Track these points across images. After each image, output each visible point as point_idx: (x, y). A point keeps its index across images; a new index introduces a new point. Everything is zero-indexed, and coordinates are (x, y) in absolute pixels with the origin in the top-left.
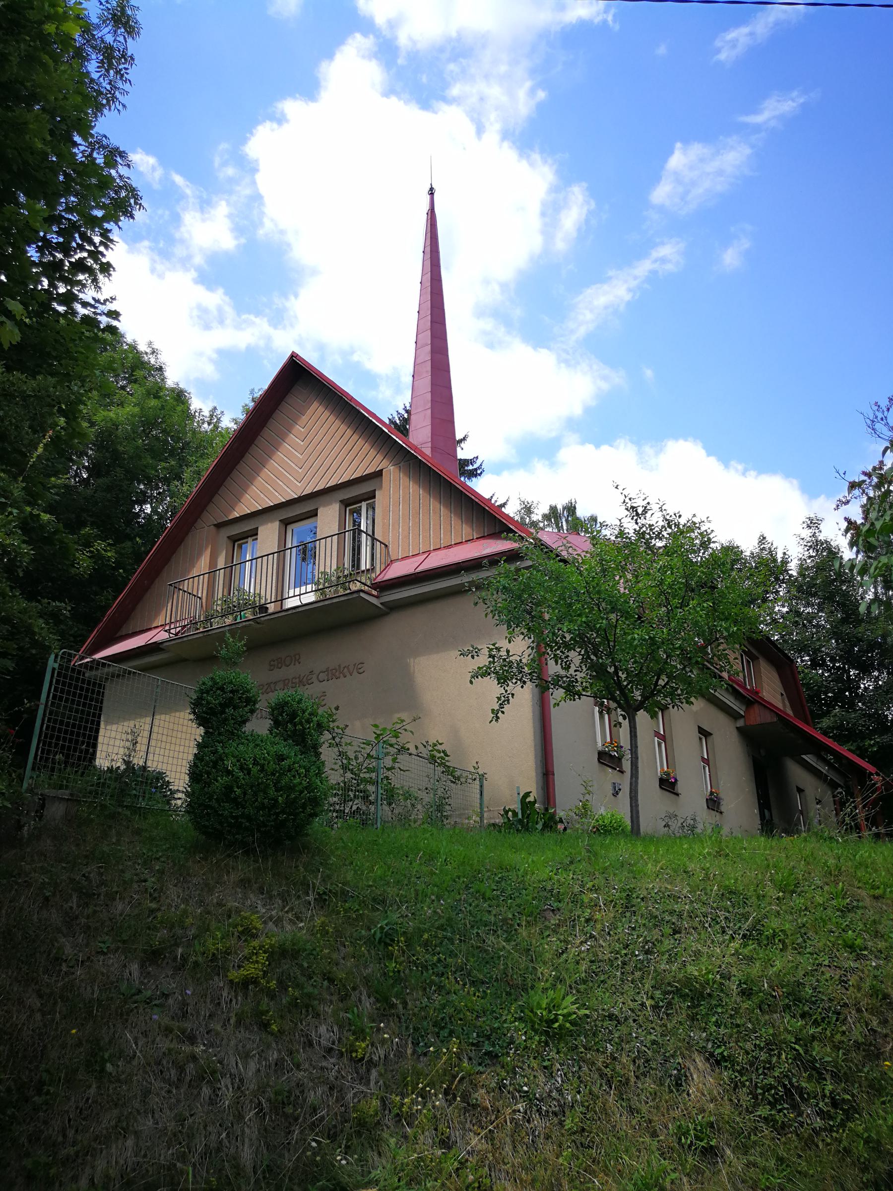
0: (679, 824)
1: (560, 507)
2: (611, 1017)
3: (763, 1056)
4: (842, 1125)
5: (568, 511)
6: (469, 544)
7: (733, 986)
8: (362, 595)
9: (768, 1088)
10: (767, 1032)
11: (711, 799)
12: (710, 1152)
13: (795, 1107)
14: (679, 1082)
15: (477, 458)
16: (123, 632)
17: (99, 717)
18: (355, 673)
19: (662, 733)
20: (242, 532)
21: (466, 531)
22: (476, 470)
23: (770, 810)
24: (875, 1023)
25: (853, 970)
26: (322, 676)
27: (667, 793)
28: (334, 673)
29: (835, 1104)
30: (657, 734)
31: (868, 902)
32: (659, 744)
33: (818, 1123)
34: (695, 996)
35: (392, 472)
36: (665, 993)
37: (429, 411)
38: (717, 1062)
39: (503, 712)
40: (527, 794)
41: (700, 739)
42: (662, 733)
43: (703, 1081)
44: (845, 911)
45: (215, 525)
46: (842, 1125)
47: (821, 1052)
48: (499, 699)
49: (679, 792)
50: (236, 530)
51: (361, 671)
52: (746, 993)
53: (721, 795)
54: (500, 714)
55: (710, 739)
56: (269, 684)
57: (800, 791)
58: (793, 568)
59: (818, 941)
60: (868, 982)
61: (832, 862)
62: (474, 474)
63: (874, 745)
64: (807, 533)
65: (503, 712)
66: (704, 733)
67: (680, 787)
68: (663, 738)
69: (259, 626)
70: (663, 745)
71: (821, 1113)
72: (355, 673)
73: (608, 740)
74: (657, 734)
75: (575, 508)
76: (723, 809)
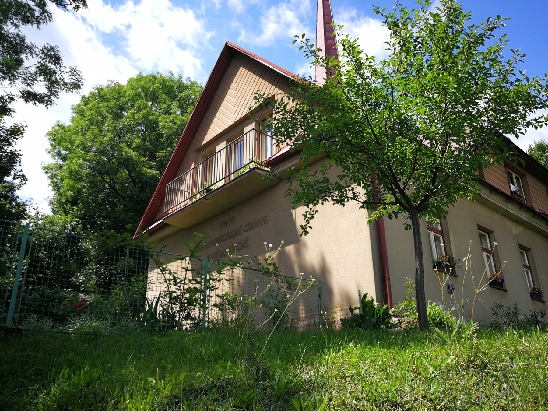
0: (505, 312)
8: (256, 170)
11: (534, 293)
16: (157, 219)
17: (148, 265)
18: (263, 223)
19: (528, 265)
20: (207, 154)
26: (246, 228)
27: (496, 290)
28: (252, 226)
30: (525, 266)
32: (527, 272)
39: (310, 227)
41: (522, 253)
42: (490, 249)
45: (196, 150)
48: (306, 216)
49: (507, 289)
50: (206, 151)
51: (266, 222)
53: (542, 290)
54: (308, 230)
55: (529, 253)
56: (220, 237)
65: (310, 227)
66: (524, 249)
68: (529, 268)
69: (208, 201)
70: (491, 258)
72: (263, 223)
73: (444, 254)
74: (525, 266)
76: (544, 299)
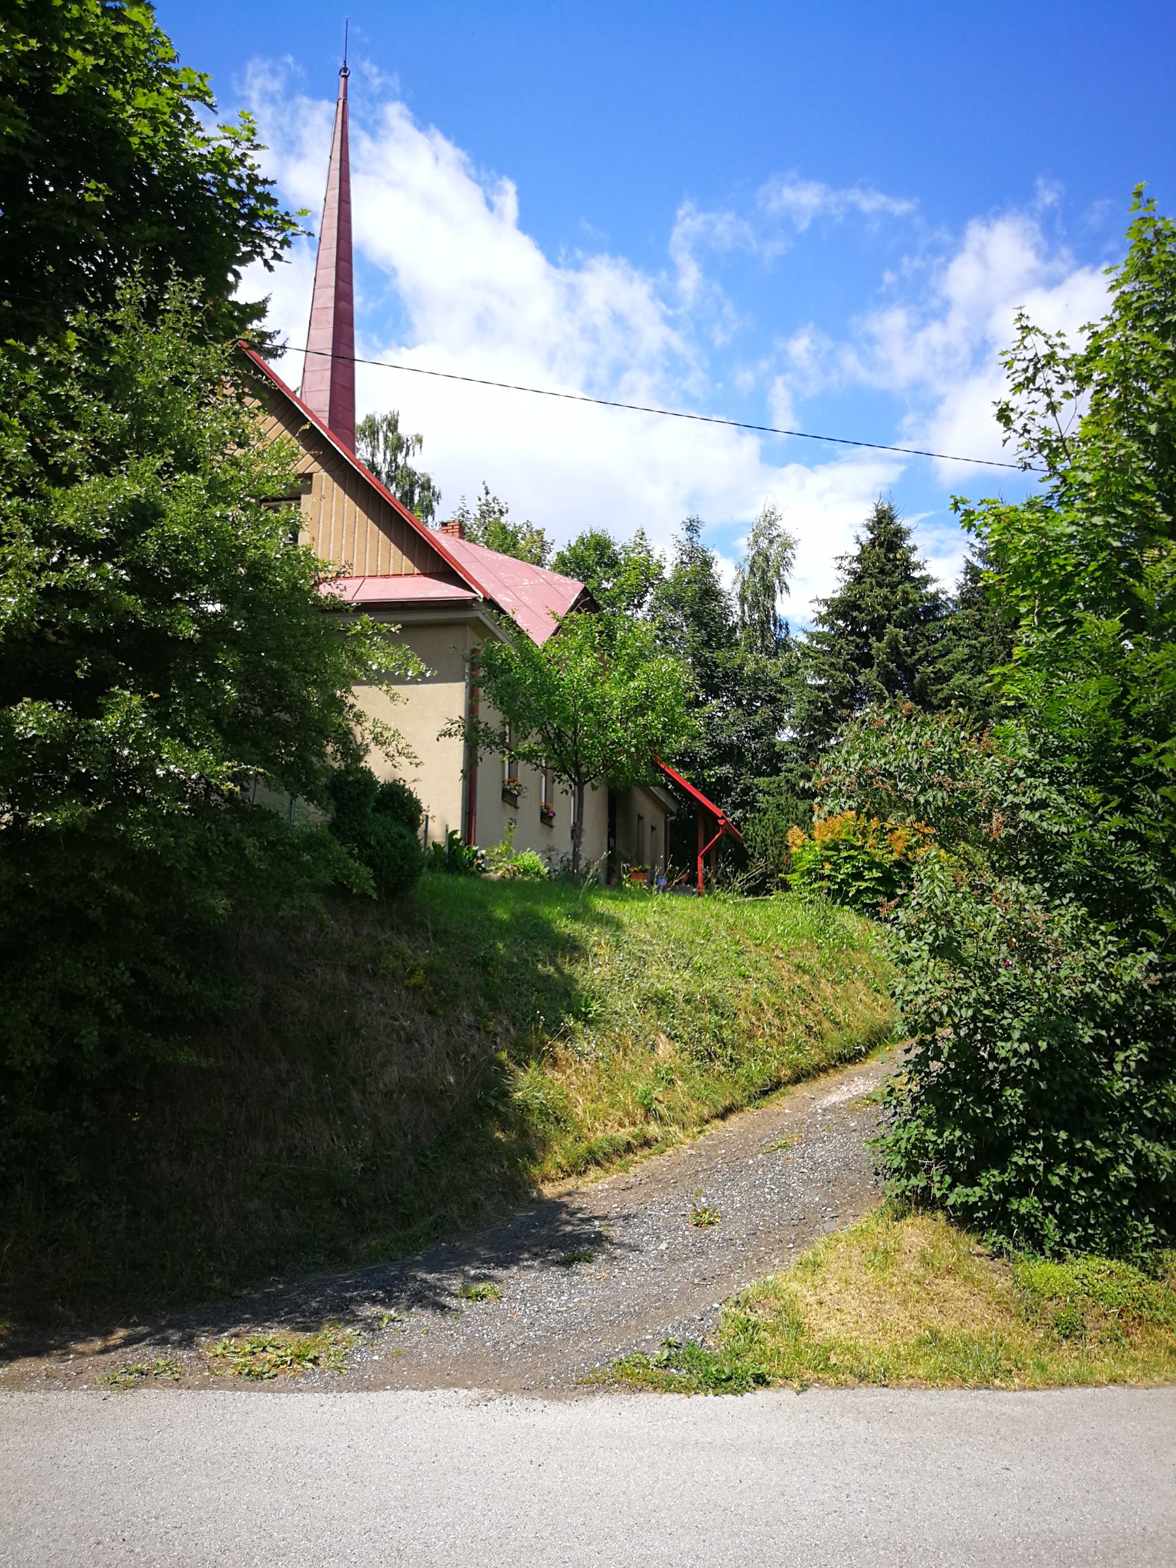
1: (378, 418)
2: (616, 1013)
3: (697, 1035)
4: (735, 1070)
5: (389, 425)
6: (409, 578)
7: (680, 997)
9: (698, 1052)
10: (699, 1023)
12: (671, 1082)
13: (711, 1060)
14: (653, 1048)
15: (279, 332)
21: (407, 564)
22: (276, 348)
23: (614, 838)
24: (754, 1020)
25: (743, 989)
29: (732, 1060)
31: (752, 948)
33: (723, 1069)
34: (661, 1001)
35: (323, 479)
36: (643, 1000)
37: (329, 373)
38: (672, 1038)
40: (455, 832)
43: (665, 1048)
44: (740, 953)
46: (735, 1070)
47: (726, 1034)
52: (688, 1002)
57: (640, 818)
58: (667, 574)
59: (724, 972)
60: (752, 996)
61: (731, 921)
62: (273, 353)
63: (713, 776)
64: (684, 535)
67: (555, 822)
71: (725, 1065)
73: (507, 777)
75: (397, 421)
